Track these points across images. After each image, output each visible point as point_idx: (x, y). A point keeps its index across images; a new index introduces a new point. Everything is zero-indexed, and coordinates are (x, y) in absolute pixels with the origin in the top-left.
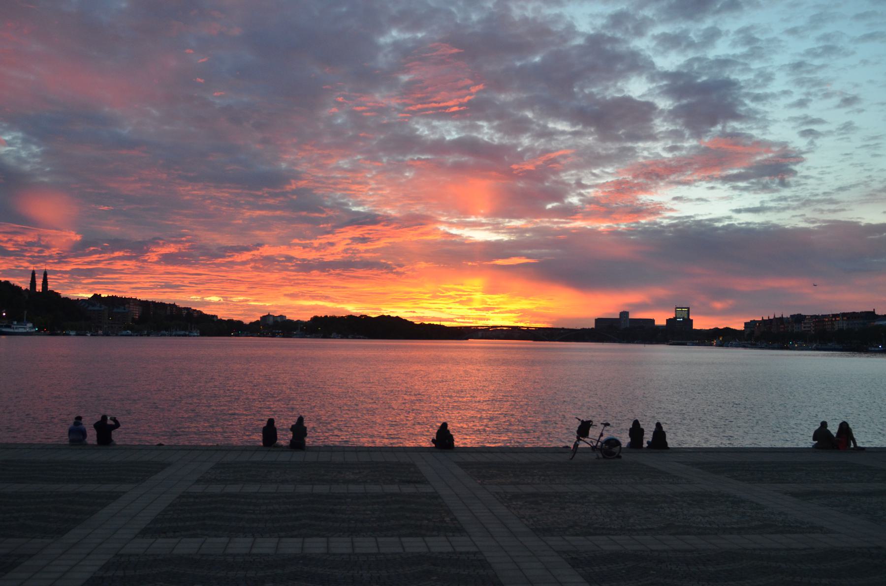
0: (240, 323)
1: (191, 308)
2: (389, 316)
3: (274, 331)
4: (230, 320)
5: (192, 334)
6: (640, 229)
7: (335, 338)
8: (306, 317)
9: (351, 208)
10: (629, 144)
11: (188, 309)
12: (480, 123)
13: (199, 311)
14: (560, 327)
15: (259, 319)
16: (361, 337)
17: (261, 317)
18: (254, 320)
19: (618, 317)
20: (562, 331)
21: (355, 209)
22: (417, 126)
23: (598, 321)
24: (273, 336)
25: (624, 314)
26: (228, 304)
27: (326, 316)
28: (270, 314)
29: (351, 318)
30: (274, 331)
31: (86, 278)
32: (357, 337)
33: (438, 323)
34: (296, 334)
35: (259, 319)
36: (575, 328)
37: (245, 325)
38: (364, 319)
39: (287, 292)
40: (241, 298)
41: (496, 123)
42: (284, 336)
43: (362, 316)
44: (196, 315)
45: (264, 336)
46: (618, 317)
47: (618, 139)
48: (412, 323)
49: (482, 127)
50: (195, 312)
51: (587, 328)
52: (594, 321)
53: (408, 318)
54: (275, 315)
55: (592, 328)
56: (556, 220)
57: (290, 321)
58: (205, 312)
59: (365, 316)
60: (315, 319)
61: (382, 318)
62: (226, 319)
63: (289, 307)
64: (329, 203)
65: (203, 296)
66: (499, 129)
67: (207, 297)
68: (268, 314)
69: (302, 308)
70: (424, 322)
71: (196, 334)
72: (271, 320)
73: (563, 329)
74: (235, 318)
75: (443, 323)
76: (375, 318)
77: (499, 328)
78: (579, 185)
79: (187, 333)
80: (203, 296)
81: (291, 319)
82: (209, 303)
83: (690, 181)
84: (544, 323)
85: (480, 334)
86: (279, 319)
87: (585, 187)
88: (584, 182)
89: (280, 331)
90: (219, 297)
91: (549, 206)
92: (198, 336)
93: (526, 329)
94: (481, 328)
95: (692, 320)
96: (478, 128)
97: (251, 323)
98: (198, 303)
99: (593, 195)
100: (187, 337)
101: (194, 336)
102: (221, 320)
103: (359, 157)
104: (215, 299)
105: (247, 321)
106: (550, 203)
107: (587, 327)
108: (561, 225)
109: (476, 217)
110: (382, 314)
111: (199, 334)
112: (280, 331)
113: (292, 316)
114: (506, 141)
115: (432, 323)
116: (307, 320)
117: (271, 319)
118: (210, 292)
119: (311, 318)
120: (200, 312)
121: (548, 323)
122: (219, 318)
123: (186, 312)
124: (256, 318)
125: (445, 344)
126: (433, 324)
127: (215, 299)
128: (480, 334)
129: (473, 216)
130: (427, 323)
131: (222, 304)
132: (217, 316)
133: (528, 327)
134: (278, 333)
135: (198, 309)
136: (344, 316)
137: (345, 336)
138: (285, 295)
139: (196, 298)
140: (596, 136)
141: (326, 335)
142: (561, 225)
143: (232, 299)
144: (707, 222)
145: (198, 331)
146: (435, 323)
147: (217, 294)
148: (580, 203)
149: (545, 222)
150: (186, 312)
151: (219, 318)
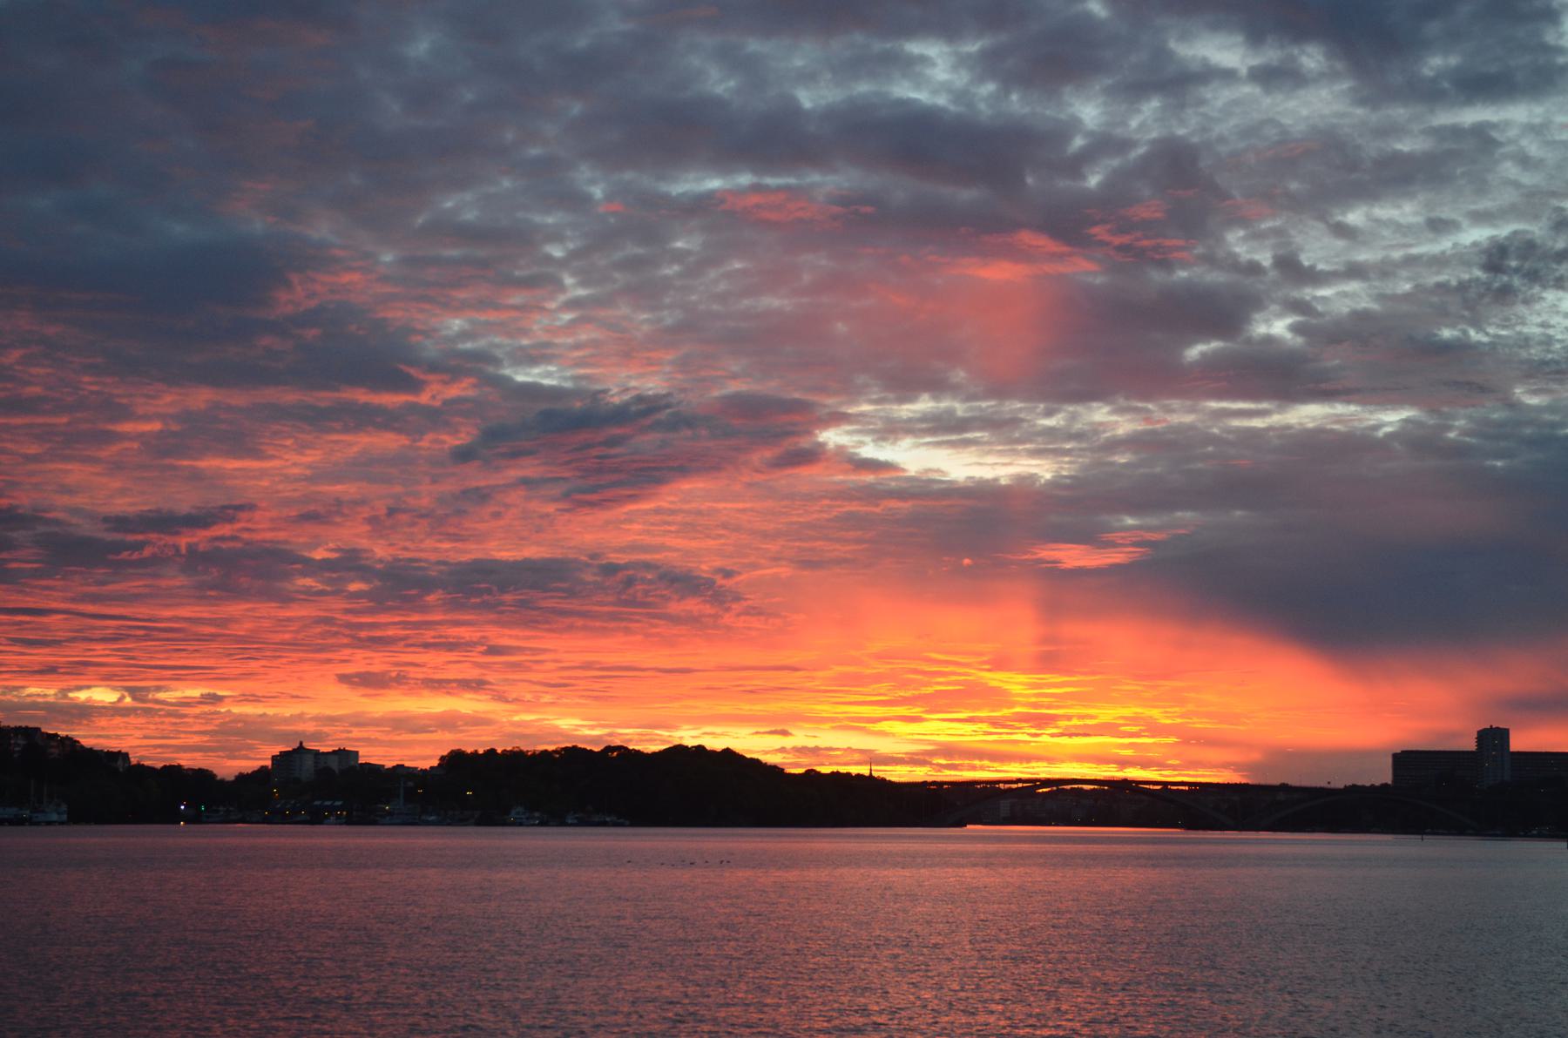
0: (203, 777)
1: (38, 729)
2: (700, 748)
3: (317, 803)
4: (172, 767)
5: (41, 817)
6: (1528, 431)
7: (521, 825)
8: (424, 755)
9: (507, 371)
10: (1471, 116)
11: (30, 733)
12: (915, 48)
13: (67, 738)
14: (1275, 781)
15: (268, 763)
16: (608, 819)
17: (274, 758)
18: (249, 765)
19: (1470, 744)
20: (1281, 797)
21: (522, 377)
22: (695, 61)
23: (1405, 761)
24: (316, 818)
25: (1494, 738)
26: (147, 712)
27: (492, 752)
28: (307, 745)
29: (574, 757)
30: (317, 803)
31: (278, 542)
32: (596, 818)
33: (864, 770)
34: (390, 813)
35: (268, 763)
36: (1323, 784)
37: (222, 782)
38: (619, 760)
39: (349, 669)
40: (195, 692)
41: (972, 47)
42: (350, 822)
43: (609, 749)
44: (55, 751)
45: (285, 820)
46: (1470, 744)
47: (1431, 94)
48: (775, 771)
49: (924, 60)
50: (53, 744)
51: (1368, 784)
52: (1390, 760)
53: (766, 753)
54: (323, 749)
55: (1385, 786)
56: (1214, 405)
57: (374, 770)
58: (87, 742)
59: (622, 749)
60: (456, 761)
61: (678, 753)
62: (159, 765)
63: (359, 721)
64: (430, 349)
65: (64, 685)
66: (988, 64)
67: (79, 688)
68: (296, 745)
69: (400, 723)
70: (818, 769)
71: (54, 817)
72: (308, 766)
73: (1284, 788)
74: (187, 761)
75: (882, 772)
76: (654, 754)
77: (1069, 787)
78: (1291, 269)
79: (26, 813)
80: (64, 685)
81: (373, 761)
82: (88, 712)
83: (339, 502)
84: (1225, 766)
85: (1005, 806)
86: (334, 764)
87: (1313, 277)
88: (1306, 260)
89: (338, 803)
90: (114, 688)
91: (1195, 351)
92: (62, 823)
93: (1159, 787)
94: (1007, 786)
95: (1478, 732)
96: (910, 66)
97: (242, 778)
98: (52, 709)
99: (1343, 308)
100: (26, 829)
101: (49, 823)
102: (140, 767)
103: (506, 183)
104: (103, 695)
105: (228, 767)
106: (1195, 342)
107: (1365, 781)
108: (1236, 423)
109: (936, 398)
110: (677, 742)
111: (65, 817)
112: (338, 803)
113: (378, 753)
114: (1017, 103)
115: (843, 769)
116: (425, 765)
117: (309, 762)
118: (80, 670)
119: (442, 758)
120: (70, 742)
121: (1237, 767)
122: (134, 761)
123: (21, 742)
124: (260, 757)
125: (865, 833)
126: (848, 774)
127: (103, 695)
128: (1005, 806)
129: (926, 396)
130: (826, 770)
131: (126, 712)
132: (127, 755)
133: (1165, 784)
134: (332, 810)
135: (62, 733)
136: (551, 748)
137: (554, 818)
138: (344, 679)
139: (40, 691)
140: (1345, 85)
141: (492, 815)
142: (1236, 423)
143: (161, 696)
144: (845, 504)
145: (64, 807)
146: (854, 770)
147: (107, 679)
148: (1300, 340)
149: (1178, 415)
150: (21, 742)
151: (134, 761)
